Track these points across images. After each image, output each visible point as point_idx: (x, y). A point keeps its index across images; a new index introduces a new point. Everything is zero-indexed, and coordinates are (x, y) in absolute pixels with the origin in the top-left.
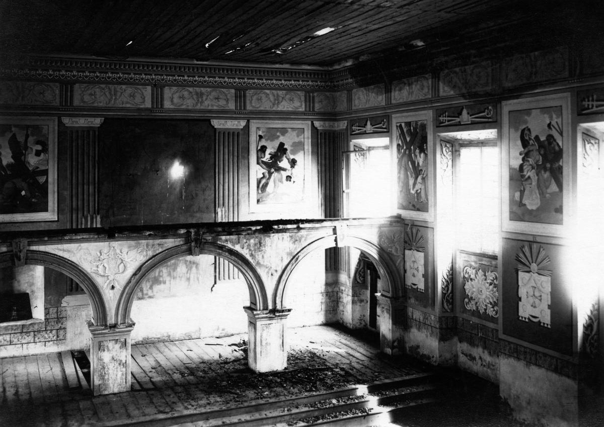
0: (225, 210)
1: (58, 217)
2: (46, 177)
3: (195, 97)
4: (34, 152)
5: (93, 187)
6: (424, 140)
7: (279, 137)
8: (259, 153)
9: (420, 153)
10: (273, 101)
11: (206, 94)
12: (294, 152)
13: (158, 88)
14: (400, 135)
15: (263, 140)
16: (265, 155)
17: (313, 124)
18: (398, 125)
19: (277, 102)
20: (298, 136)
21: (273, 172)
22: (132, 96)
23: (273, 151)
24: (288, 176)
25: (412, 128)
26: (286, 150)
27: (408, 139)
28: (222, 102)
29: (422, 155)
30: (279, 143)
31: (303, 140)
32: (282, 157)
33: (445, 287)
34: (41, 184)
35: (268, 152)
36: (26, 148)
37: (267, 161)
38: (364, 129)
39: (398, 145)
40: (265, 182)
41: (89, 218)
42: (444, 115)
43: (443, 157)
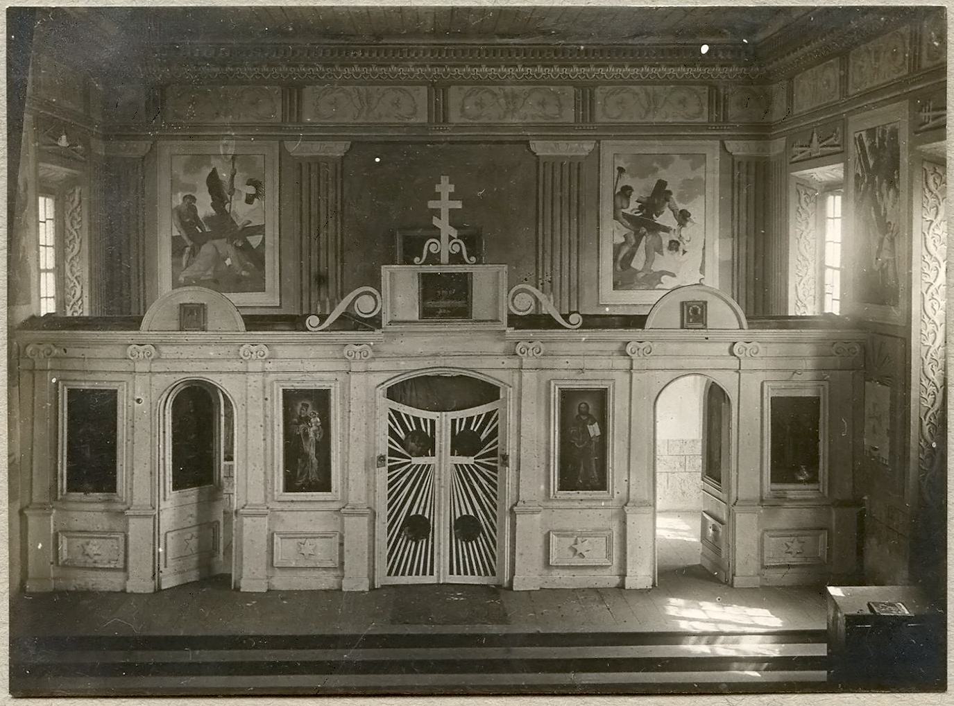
0: (554, 298)
1: (280, 301)
2: (262, 236)
3: (502, 101)
4: (244, 197)
5: (334, 254)
6: (895, 164)
7: (656, 170)
8: (618, 200)
9: (888, 189)
10: (646, 106)
11: (523, 96)
12: (685, 197)
13: (438, 88)
14: (859, 155)
15: (626, 176)
16: (629, 203)
17: (723, 147)
18: (857, 135)
19: (652, 107)
20: (693, 169)
21: (644, 234)
22: (396, 104)
23: (645, 195)
24: (673, 241)
25: (877, 139)
26: (670, 193)
27: (871, 163)
28: (551, 110)
29: (891, 192)
30: (655, 181)
31: (703, 176)
32: (663, 206)
33: (926, 457)
34: (255, 247)
35: (634, 197)
36: (232, 191)
37: (633, 213)
38: (809, 150)
39: (857, 176)
40: (629, 252)
41: (328, 304)
42: (927, 108)
43: (928, 195)
